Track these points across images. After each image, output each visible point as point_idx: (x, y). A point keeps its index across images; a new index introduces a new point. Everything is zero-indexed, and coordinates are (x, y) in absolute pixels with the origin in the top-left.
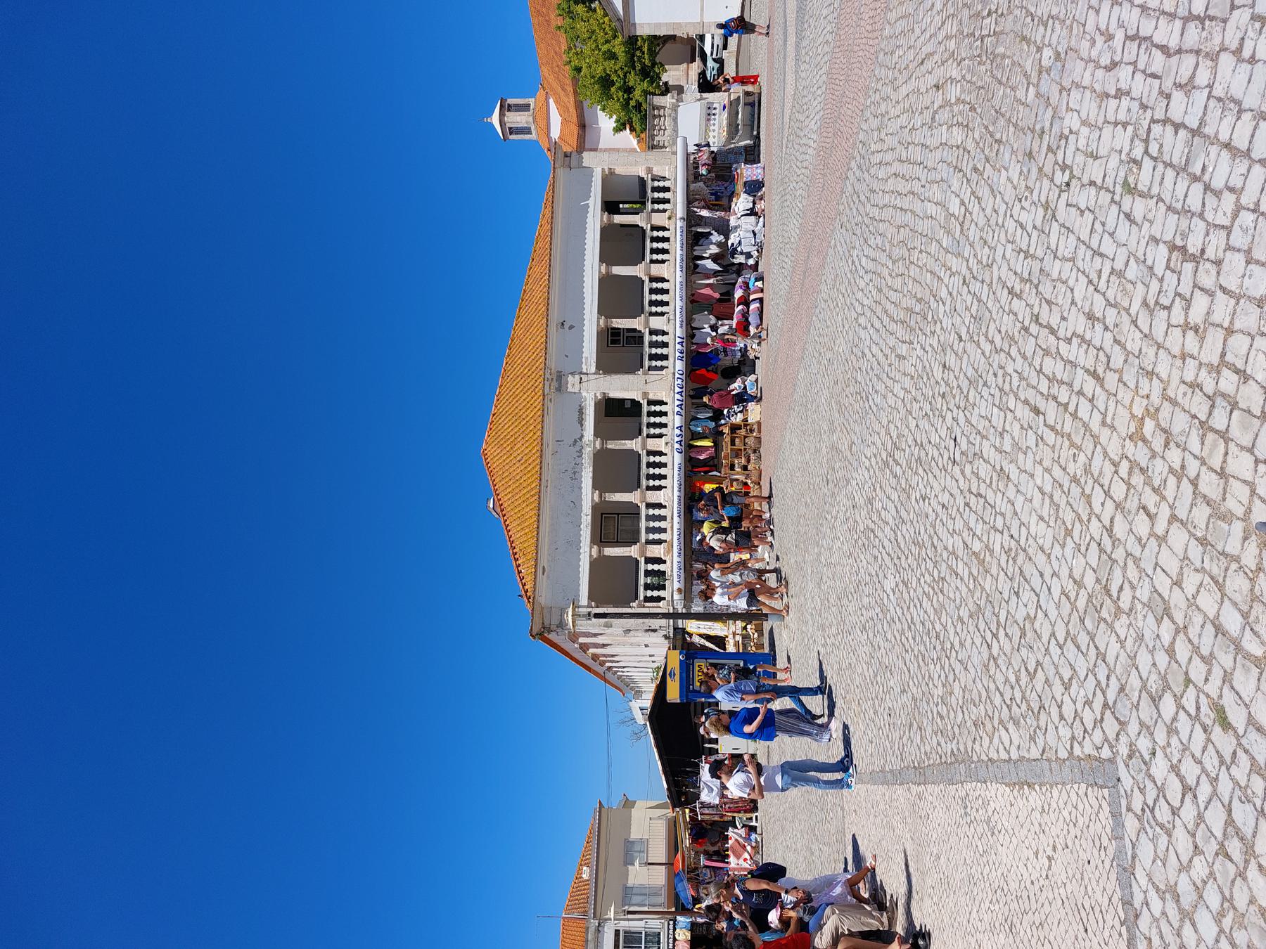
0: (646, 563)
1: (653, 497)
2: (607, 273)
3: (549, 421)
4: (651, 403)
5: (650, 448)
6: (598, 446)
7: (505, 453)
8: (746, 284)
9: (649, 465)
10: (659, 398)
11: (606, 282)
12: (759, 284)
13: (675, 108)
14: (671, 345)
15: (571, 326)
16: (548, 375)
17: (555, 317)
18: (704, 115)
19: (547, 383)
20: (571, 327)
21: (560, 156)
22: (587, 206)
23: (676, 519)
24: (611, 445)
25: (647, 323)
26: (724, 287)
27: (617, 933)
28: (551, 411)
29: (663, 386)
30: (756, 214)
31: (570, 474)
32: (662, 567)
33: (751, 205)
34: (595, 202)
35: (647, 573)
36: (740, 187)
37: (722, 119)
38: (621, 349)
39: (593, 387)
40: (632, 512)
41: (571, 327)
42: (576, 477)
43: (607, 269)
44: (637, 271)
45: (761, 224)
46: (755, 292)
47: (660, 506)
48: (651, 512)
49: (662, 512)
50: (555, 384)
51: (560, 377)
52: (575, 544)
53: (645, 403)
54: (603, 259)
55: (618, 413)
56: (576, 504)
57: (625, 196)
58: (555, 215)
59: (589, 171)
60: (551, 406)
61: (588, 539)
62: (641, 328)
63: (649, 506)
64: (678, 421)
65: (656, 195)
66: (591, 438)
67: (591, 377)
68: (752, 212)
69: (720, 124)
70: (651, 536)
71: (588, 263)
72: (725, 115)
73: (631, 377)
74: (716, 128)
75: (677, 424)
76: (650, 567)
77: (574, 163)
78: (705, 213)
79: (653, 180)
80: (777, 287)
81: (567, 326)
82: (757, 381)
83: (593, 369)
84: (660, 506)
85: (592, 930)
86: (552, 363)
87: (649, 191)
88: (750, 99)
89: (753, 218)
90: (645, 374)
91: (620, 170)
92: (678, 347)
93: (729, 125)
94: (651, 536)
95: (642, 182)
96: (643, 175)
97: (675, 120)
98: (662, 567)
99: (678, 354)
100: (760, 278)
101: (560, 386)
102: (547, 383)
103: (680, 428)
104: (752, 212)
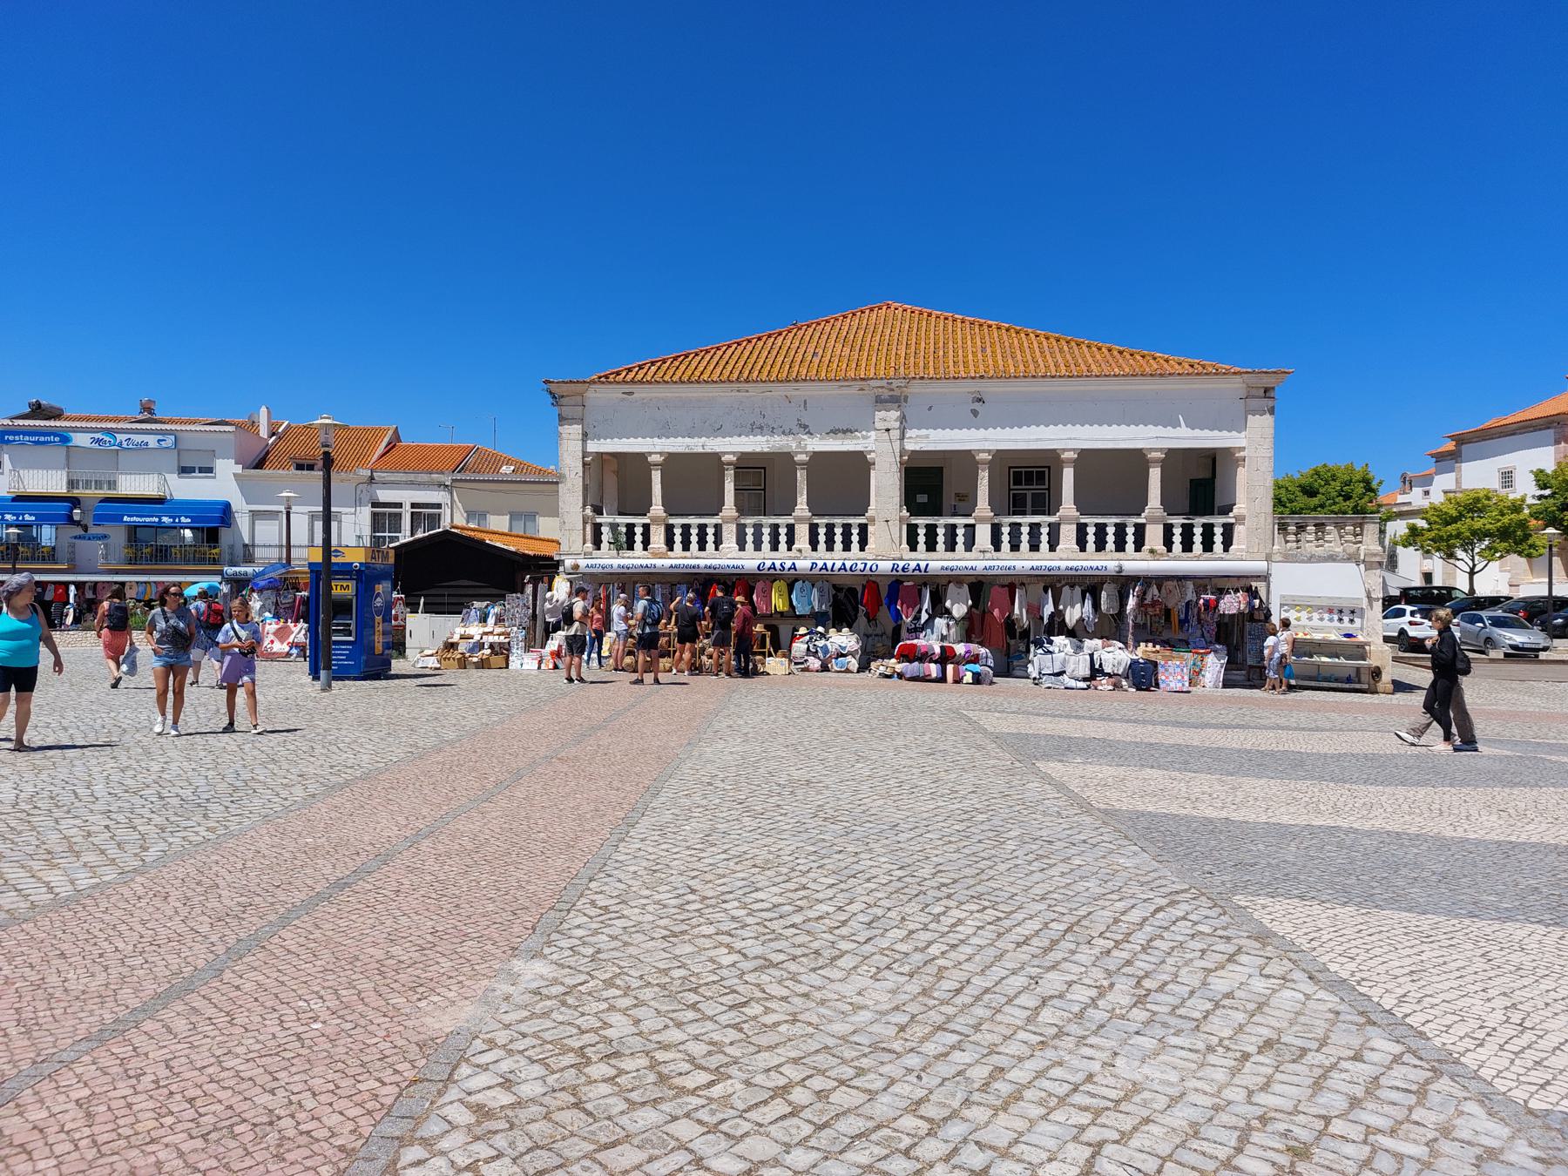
0: (1225, 526)
1: (1068, 534)
2: (795, 463)
3: (831, 390)
4: (863, 529)
5: (652, 528)
6: (798, 458)
7: (892, 330)
8: (975, 659)
9: (775, 528)
10: (871, 539)
11: (1135, 461)
12: (968, 677)
13: (1353, 558)
14: (774, 554)
15: (977, 411)
16: (895, 383)
17: (989, 388)
18: (1339, 604)
19: (884, 383)
20: (975, 413)
21: (1267, 381)
22: (1176, 425)
23: (667, 562)
24: (801, 475)
25: (982, 520)
26: (1005, 630)
27: (439, 506)
28: (845, 391)
29: (885, 549)
30: (1092, 677)
31: (760, 421)
32: (638, 545)
33: (1107, 669)
34: (1187, 437)
35: (631, 527)
36: (1144, 651)
37: (1330, 631)
38: (929, 486)
39: (883, 448)
40: (1046, 503)
41: (975, 413)
42: (756, 429)
43: (1069, 461)
44: (1068, 507)
45: (1073, 683)
46: (956, 672)
47: (718, 542)
48: (710, 531)
49: (710, 546)
50: (886, 394)
51: (896, 401)
52: (665, 431)
53: (862, 520)
54: (1084, 454)
55: (841, 484)
56: (718, 431)
57: (1201, 487)
58: (1157, 380)
59: (1241, 427)
60: (854, 391)
61: (672, 450)
62: (1061, 512)
63: (718, 528)
64: (803, 565)
65: (1198, 531)
66: (809, 449)
67: (897, 445)
68: (1096, 672)
69: (1315, 629)
70: (678, 531)
71: (991, 433)
72: (1333, 637)
73: (897, 500)
74: (1316, 622)
75: (799, 564)
76: (639, 530)
77: (1254, 403)
78: (1132, 602)
79: (1225, 526)
80: (1004, 708)
81: (977, 406)
82: (848, 671)
83: (910, 446)
84: (718, 542)
85: (442, 478)
86: (916, 388)
87: (1204, 520)
88: (1365, 677)
89: (1087, 673)
90: (901, 520)
91: (1242, 474)
92: (913, 564)
93: (1312, 643)
94: (678, 531)
95: (1226, 510)
96: (1236, 510)
97: (1332, 558)
98: (638, 545)
99: (901, 564)
100: (977, 679)
101: (886, 401)
102: (884, 383)
103: (794, 567)
104: (1096, 672)
